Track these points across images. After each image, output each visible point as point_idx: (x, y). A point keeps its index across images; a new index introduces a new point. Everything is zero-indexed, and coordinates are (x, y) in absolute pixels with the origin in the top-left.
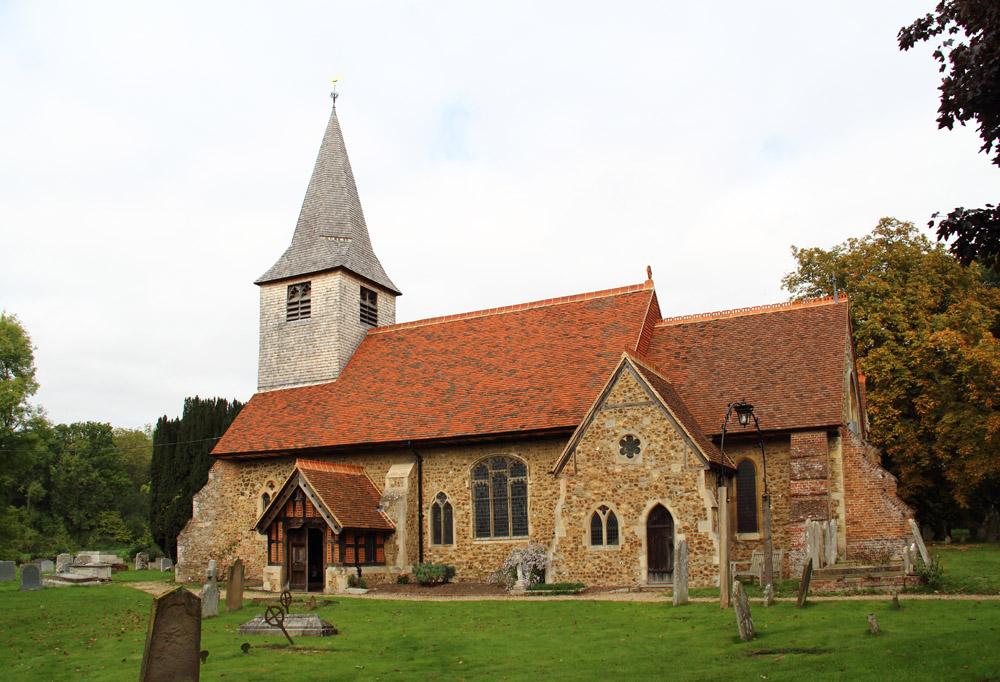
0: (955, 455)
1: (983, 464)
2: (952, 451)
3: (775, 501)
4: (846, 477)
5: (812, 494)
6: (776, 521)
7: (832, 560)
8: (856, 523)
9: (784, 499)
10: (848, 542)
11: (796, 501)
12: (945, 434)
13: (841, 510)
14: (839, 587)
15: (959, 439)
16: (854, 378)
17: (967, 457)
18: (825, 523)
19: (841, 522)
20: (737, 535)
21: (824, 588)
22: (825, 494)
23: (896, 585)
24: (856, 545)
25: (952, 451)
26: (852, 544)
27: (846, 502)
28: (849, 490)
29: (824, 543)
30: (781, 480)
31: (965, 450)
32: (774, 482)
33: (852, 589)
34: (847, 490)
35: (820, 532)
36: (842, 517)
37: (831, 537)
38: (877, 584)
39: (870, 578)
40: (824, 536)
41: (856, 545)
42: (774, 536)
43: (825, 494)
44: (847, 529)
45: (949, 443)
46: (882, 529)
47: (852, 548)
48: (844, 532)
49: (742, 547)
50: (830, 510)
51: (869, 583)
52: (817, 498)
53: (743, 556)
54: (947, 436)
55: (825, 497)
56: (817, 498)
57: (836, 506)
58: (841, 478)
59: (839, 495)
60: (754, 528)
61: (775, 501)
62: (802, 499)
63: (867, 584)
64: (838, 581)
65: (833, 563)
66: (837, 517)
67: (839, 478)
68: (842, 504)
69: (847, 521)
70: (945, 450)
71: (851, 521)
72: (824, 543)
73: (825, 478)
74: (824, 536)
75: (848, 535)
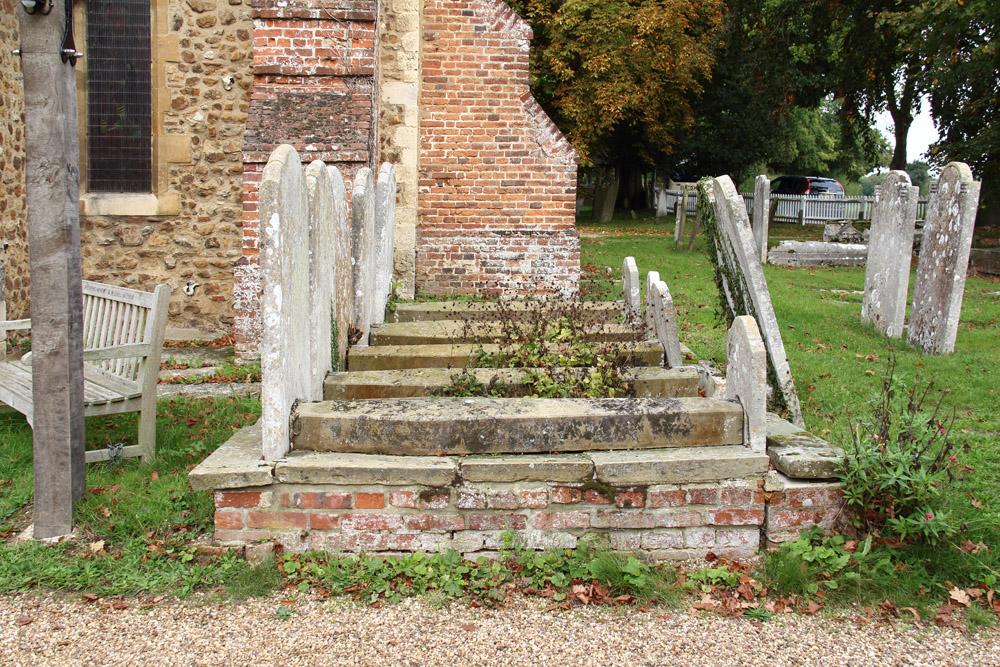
0: (580, 73)
1: (623, 91)
2: (575, 62)
3: (210, 96)
4: (428, 38)
5: (321, 74)
6: (211, 159)
7: (374, 310)
8: (446, 179)
9: (238, 92)
10: (423, 232)
11: (270, 91)
12: (566, 32)
13: (407, 137)
14: (428, 526)
15: (587, 44)
16: (335, 309)
17: (604, 77)
18: (362, 173)
19: (405, 173)
20: (86, 198)
21: (349, 529)
22: (368, 76)
23: (723, 524)
24: (443, 245)
25: (575, 62)
26: (432, 243)
27: (422, 116)
28: (432, 76)
29: (355, 252)
30: (231, 30)
31: (598, 63)
32: (209, 33)
33: (495, 538)
34: (427, 79)
35: (341, 205)
36: (410, 159)
37: (379, 224)
38: (629, 517)
39: (594, 487)
40: (356, 223)
41: (443, 245)
42: (205, 206)
43: (368, 76)
44: (421, 197)
45: (573, 46)
46: (521, 200)
47: (433, 254)
48: (413, 206)
49: (101, 236)
50: (378, 133)
51: (587, 514)
52: (339, 88)
53: (104, 264)
54: (570, 35)
55: (363, 86)
56: (339, 88)
57: (394, 123)
58: (412, 39)
59: (402, 92)
60: (140, 179)
61: (210, 96)
62: (292, 89)
63: (576, 516)
64: (426, 496)
65: (380, 318)
66: (395, 158)
67: (405, 38)
68: (412, 119)
69: (423, 172)
70: (565, 59)
71: (435, 176)
72: (355, 252)
73: (369, 22)
74: (356, 223)
75: (421, 214)
